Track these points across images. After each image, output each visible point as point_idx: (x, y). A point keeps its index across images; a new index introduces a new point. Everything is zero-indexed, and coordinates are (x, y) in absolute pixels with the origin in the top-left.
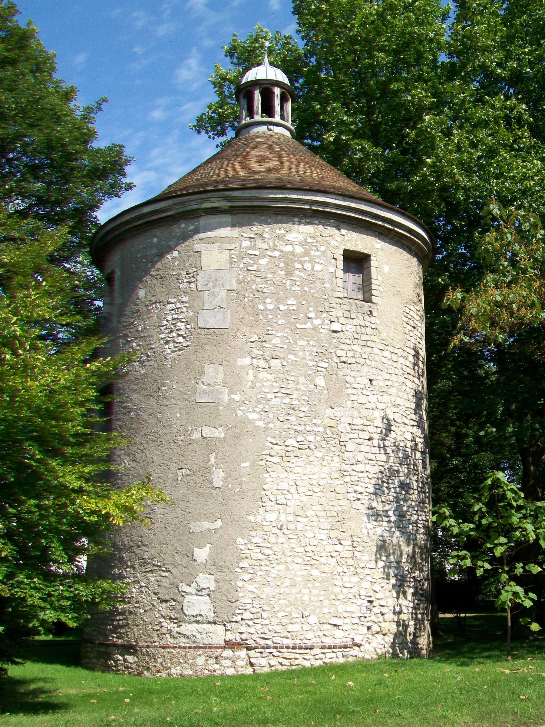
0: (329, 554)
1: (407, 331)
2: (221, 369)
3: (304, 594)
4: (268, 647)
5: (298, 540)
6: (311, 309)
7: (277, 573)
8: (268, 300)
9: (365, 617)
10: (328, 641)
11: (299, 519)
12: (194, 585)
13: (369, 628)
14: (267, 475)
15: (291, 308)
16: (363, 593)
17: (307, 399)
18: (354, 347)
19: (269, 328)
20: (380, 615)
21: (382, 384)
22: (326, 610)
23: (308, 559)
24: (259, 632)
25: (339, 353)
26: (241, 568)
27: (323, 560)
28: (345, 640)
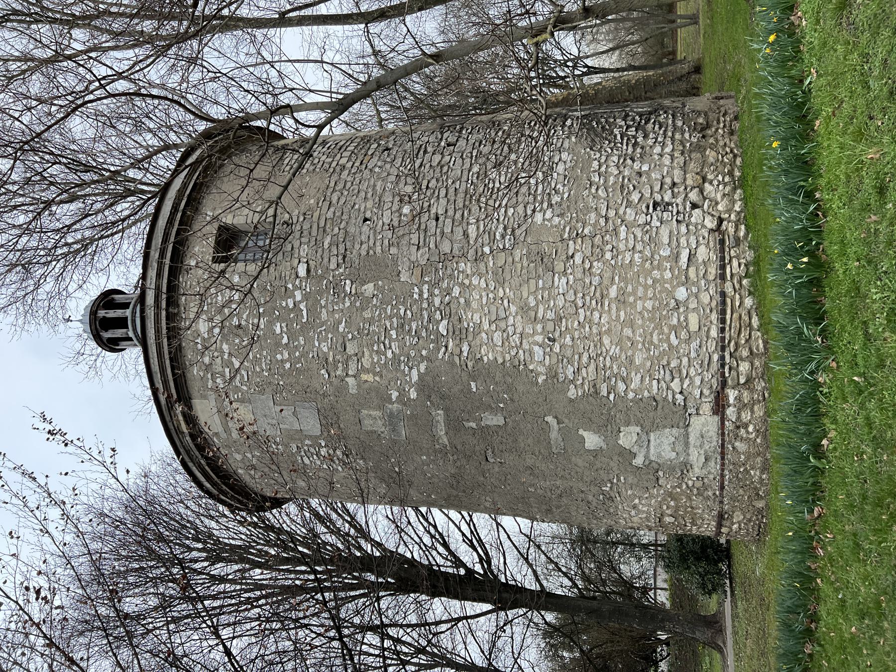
0: (587, 273)
1: (312, 168)
2: (365, 412)
3: (644, 308)
4: (722, 358)
5: (568, 317)
6: (284, 304)
7: (614, 347)
8: (279, 357)
9: (678, 212)
10: (713, 271)
11: (540, 315)
12: (635, 450)
13: (694, 206)
14: (485, 358)
15: (285, 329)
16: (642, 219)
17: (389, 307)
18: (326, 245)
19: (311, 356)
20: (676, 190)
21: (369, 204)
22: (668, 275)
23: (594, 302)
24: (700, 371)
25: (333, 266)
26: (609, 393)
27: (596, 280)
28: (712, 244)
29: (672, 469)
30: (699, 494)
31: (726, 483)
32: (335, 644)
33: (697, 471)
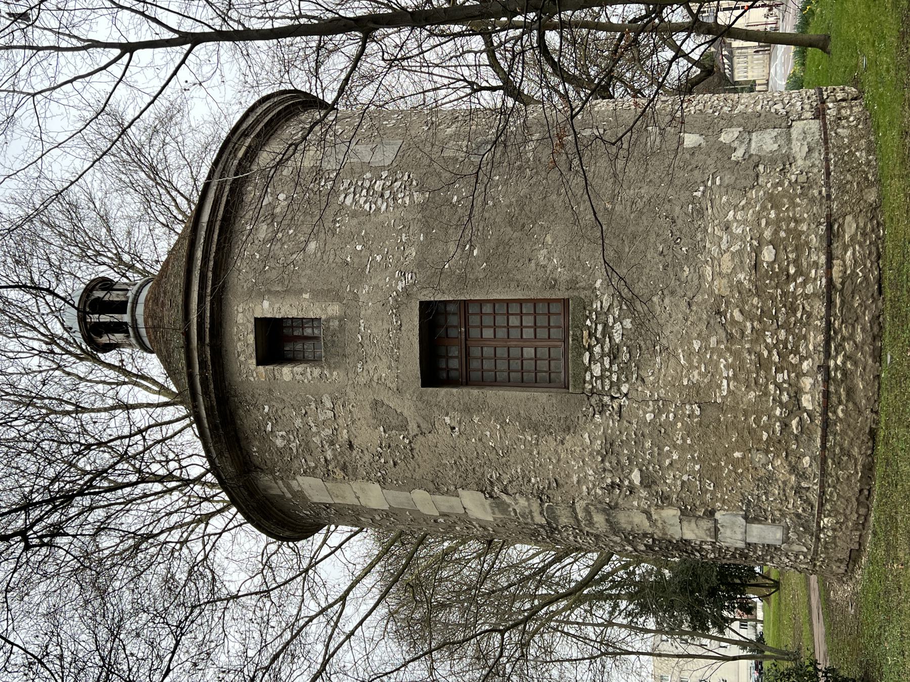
29: (773, 161)
30: (803, 195)
31: (832, 168)
32: (122, 637)
33: (800, 162)
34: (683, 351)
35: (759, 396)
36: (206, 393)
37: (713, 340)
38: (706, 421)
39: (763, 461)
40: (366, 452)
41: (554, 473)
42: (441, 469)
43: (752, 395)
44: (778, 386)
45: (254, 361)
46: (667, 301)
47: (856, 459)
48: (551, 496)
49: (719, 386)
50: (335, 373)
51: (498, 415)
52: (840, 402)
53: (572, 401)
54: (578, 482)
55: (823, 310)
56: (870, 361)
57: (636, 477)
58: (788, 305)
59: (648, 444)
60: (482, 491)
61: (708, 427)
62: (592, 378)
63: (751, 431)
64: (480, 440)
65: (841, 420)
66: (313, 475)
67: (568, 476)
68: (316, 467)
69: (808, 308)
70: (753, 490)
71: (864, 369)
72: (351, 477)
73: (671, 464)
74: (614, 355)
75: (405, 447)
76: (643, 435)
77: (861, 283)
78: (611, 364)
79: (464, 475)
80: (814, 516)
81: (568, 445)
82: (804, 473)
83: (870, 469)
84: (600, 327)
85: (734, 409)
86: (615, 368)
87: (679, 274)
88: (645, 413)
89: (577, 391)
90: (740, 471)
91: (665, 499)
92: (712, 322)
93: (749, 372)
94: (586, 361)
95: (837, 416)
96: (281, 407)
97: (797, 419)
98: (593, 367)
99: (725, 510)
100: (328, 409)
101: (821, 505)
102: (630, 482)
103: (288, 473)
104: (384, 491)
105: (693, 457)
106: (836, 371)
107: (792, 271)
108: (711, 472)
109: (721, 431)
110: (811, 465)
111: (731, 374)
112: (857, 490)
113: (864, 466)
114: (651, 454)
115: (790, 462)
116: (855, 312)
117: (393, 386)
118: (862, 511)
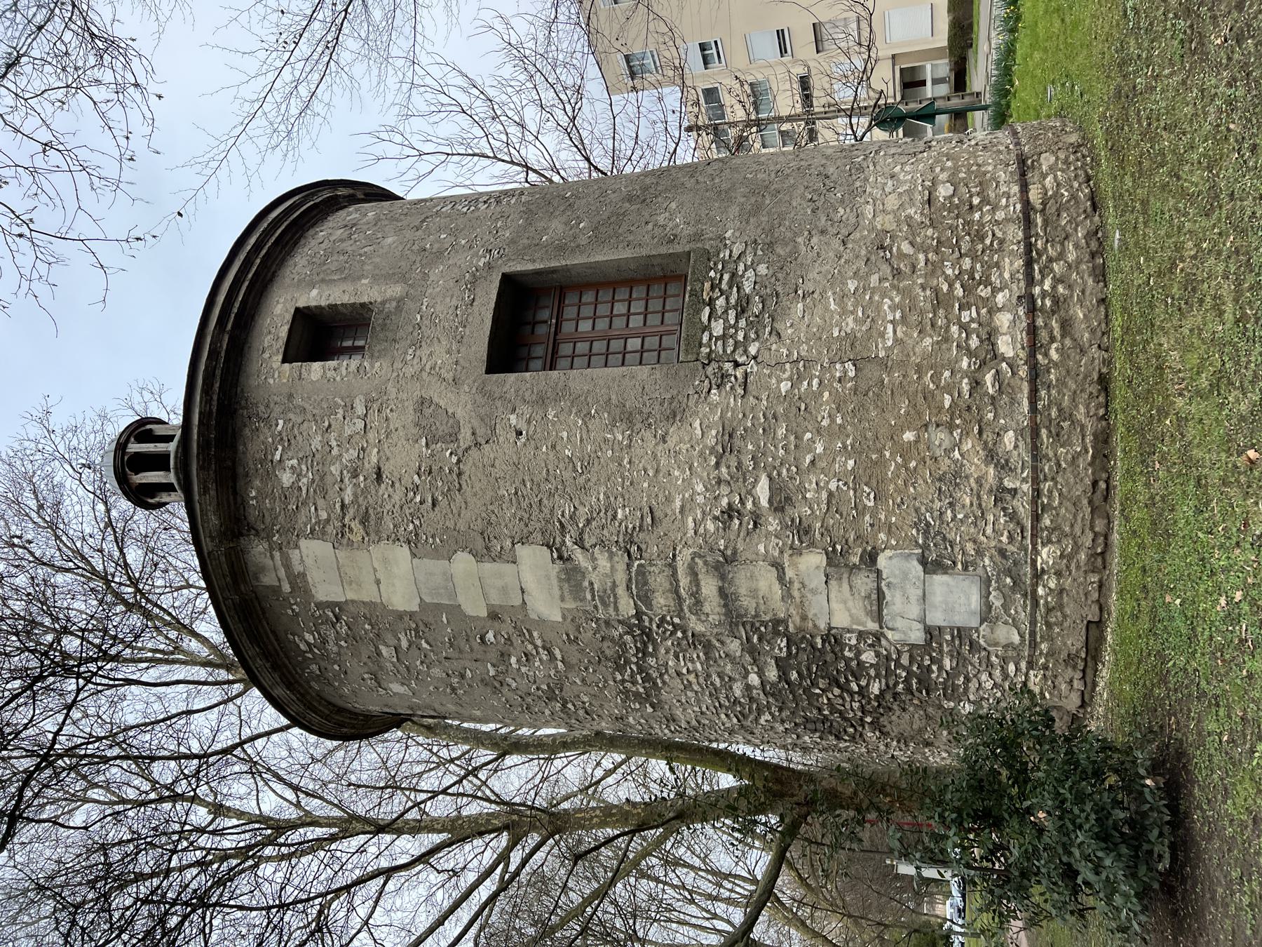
34: (834, 293)
35: (938, 342)
36: (207, 390)
37: (874, 279)
38: (863, 386)
39: (946, 444)
40: (397, 485)
41: (649, 496)
42: (494, 507)
43: (928, 341)
44: (964, 327)
45: (280, 357)
46: (815, 240)
47: (1083, 427)
48: (643, 547)
49: (882, 335)
50: (377, 364)
51: (580, 405)
52: (1053, 339)
53: (682, 373)
54: (682, 507)
55: (1020, 234)
56: (1090, 281)
57: (763, 491)
58: (973, 233)
59: (781, 431)
60: (549, 547)
61: (866, 395)
62: (710, 339)
63: (927, 396)
64: (554, 447)
65: (1056, 365)
66: (323, 536)
67: (669, 499)
68: (328, 521)
69: (999, 234)
70: (932, 501)
71: (1083, 292)
72: (373, 535)
73: (813, 462)
74: (742, 308)
75: (451, 470)
76: (775, 417)
77: (1068, 201)
78: (737, 318)
79: (526, 516)
80: (1026, 550)
81: (671, 441)
82: (1007, 461)
83: (1106, 441)
84: (726, 277)
85: (903, 364)
86: (742, 323)
87: (832, 215)
88: (779, 381)
89: (691, 357)
90: (913, 464)
91: (803, 530)
92: (873, 258)
93: (922, 313)
94: (705, 318)
95: (1051, 360)
96: (299, 421)
97: (993, 371)
98: (713, 324)
99: (893, 548)
100: (359, 417)
101: (1036, 518)
102: (754, 503)
103: (292, 535)
104: (416, 561)
105: (845, 447)
106: (1043, 299)
107: (976, 201)
108: (870, 475)
109: (885, 398)
110: (1016, 447)
111: (898, 315)
112: (1088, 482)
113: (1095, 435)
114: (785, 448)
115: (986, 443)
116: (1064, 229)
117: (449, 376)
118: (1100, 526)
